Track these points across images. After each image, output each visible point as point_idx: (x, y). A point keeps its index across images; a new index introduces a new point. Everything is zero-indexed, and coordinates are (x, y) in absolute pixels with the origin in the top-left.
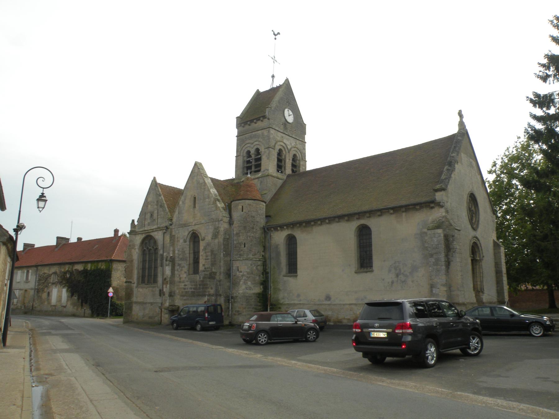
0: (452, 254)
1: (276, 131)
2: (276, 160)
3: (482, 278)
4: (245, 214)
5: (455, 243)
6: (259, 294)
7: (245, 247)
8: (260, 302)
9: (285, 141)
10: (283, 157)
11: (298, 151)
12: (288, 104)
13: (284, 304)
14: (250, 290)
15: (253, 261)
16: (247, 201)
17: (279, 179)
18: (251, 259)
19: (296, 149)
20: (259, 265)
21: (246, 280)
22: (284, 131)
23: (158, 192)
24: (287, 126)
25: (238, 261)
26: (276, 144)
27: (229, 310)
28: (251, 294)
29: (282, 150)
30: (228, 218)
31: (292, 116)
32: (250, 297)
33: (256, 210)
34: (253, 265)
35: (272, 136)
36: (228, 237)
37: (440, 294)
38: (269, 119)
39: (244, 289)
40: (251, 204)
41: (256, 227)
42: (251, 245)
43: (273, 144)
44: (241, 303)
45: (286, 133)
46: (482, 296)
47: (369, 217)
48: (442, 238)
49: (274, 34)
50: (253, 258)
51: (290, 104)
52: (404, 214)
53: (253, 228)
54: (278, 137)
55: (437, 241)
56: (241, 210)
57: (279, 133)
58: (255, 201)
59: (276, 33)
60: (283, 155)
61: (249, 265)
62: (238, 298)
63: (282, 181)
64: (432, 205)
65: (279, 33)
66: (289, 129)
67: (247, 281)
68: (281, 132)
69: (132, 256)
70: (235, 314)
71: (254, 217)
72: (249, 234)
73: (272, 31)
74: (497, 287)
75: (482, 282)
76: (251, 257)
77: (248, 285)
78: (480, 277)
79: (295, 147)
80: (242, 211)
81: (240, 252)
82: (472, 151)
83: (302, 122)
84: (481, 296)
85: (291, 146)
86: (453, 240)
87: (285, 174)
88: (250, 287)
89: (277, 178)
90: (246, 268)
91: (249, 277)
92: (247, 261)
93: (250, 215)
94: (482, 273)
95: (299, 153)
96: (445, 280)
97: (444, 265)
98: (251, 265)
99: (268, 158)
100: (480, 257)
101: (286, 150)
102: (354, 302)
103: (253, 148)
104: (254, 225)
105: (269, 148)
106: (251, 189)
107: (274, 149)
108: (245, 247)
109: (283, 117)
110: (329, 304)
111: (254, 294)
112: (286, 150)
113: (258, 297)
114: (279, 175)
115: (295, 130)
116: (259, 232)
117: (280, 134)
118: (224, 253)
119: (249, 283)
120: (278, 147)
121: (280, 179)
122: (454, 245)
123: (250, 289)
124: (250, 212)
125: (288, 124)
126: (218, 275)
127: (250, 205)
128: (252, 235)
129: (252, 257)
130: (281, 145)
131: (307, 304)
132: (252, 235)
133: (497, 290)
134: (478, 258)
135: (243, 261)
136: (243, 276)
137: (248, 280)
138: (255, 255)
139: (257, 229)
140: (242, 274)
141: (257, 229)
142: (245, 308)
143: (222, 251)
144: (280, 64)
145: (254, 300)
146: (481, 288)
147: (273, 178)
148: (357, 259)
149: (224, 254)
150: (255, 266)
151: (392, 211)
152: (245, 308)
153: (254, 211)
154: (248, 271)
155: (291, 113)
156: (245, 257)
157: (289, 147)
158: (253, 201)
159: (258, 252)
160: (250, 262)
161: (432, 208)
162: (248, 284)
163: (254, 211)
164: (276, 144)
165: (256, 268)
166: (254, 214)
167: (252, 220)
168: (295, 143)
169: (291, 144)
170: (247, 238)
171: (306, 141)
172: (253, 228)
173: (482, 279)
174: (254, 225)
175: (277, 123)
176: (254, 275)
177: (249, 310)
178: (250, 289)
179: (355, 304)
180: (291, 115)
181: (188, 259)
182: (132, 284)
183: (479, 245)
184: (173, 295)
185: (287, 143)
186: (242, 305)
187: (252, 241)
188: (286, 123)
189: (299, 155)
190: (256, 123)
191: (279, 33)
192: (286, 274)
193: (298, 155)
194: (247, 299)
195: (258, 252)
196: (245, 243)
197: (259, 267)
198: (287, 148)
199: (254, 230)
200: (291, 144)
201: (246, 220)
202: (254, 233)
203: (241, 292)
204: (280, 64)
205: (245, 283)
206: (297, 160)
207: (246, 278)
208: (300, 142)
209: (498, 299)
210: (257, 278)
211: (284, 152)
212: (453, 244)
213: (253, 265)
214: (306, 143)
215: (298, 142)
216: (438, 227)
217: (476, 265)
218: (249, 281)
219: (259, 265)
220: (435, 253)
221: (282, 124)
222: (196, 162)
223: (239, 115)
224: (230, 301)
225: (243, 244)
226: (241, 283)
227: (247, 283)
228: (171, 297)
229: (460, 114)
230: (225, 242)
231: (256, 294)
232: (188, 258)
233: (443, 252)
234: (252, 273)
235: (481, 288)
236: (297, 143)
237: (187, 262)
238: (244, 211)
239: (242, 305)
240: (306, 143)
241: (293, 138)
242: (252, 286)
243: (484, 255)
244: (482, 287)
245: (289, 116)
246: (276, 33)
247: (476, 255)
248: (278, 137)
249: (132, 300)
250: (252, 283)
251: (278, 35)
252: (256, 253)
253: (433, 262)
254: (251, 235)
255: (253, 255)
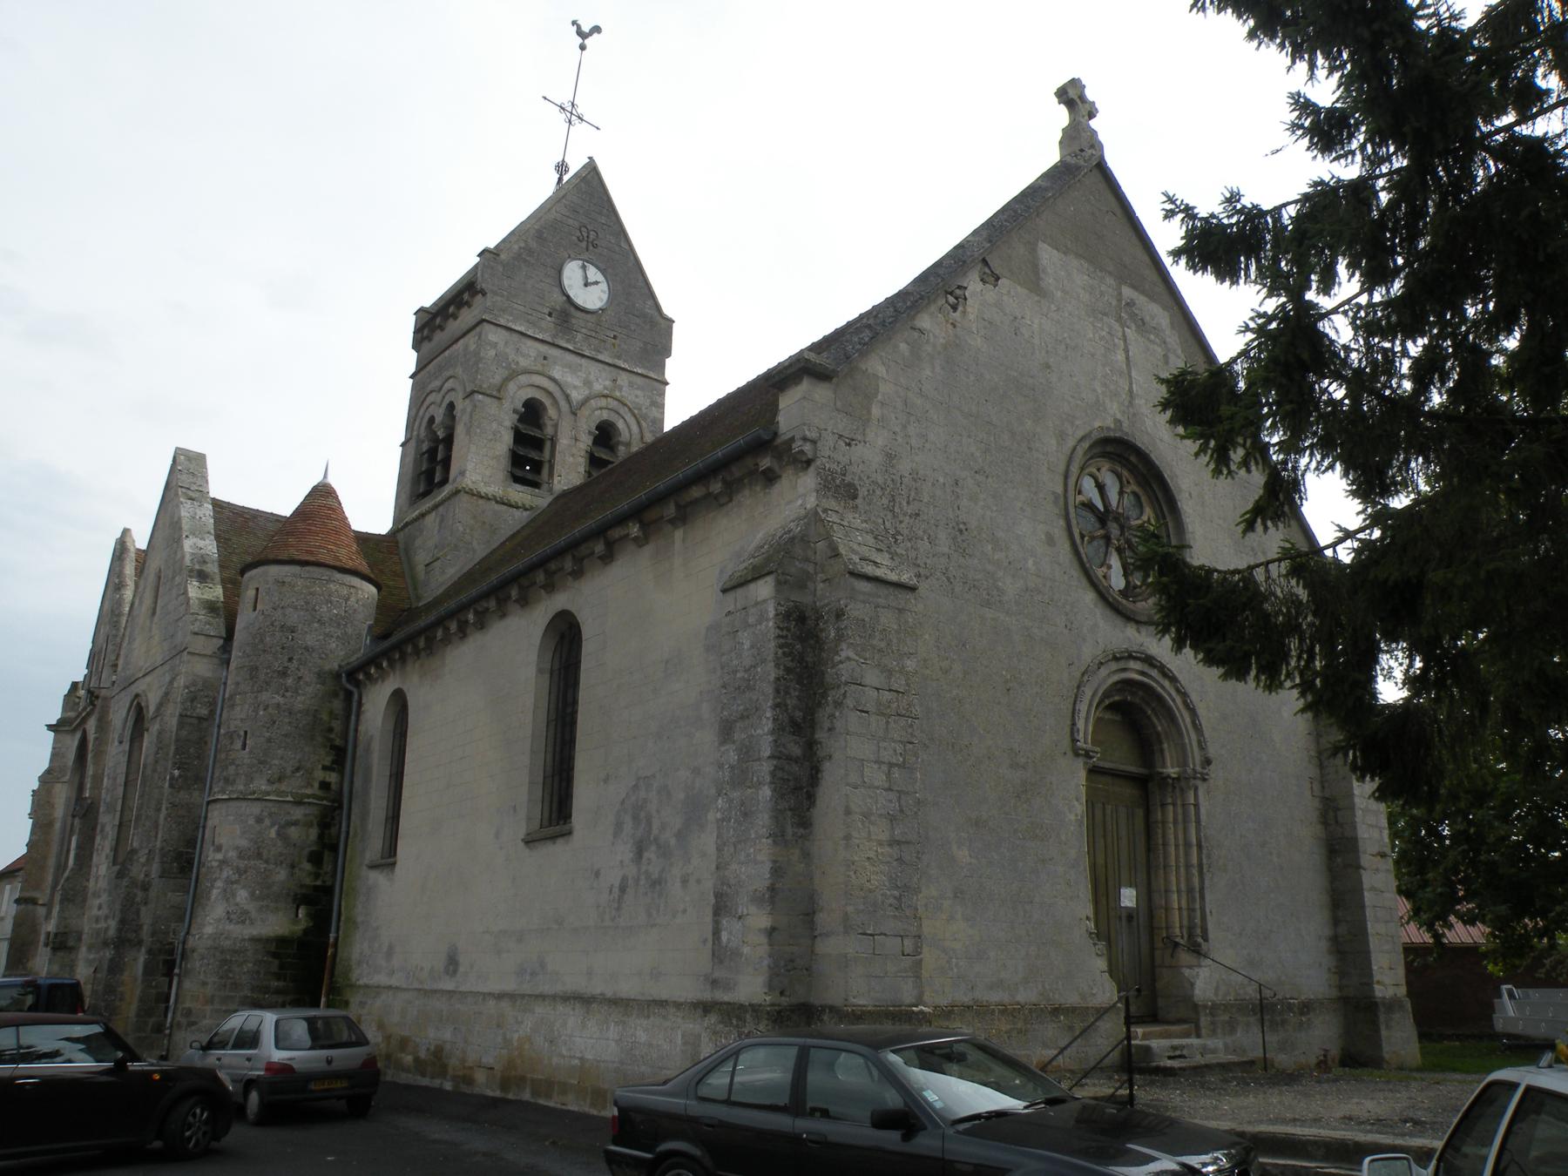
0: (832, 716)
1: (515, 337)
2: (507, 438)
3: (1195, 872)
4: (261, 618)
5: (843, 654)
6: (281, 941)
7: (244, 747)
8: (278, 977)
9: (557, 373)
10: (549, 430)
11: (621, 412)
12: (584, 244)
13: (367, 986)
14: (243, 922)
15: (270, 804)
16: (274, 570)
17: (511, 506)
18: (260, 796)
19: (613, 404)
20: (295, 823)
21: (232, 883)
22: (555, 336)
23: (118, 577)
24: (574, 321)
25: (218, 806)
26: (507, 379)
27: (167, 1008)
28: (244, 940)
29: (541, 403)
30: (215, 640)
31: (604, 286)
32: (235, 952)
33: (307, 603)
34: (267, 822)
35: (492, 353)
36: (204, 712)
37: (746, 950)
38: (484, 294)
39: (219, 920)
40: (286, 580)
41: (298, 669)
42: (269, 740)
43: (497, 379)
44: (202, 977)
45: (565, 345)
46: (1190, 967)
47: (578, 574)
48: (771, 624)
49: (580, 33)
50: (268, 793)
51: (595, 246)
52: (679, 534)
53: (284, 674)
54: (526, 356)
55: (752, 647)
56: (252, 605)
57: (530, 343)
58: (307, 568)
59: (586, 29)
60: (549, 423)
61: (251, 821)
62: (195, 954)
63: (526, 514)
64: (766, 462)
65: (597, 29)
66: (583, 330)
67: (235, 886)
68: (536, 339)
69: (53, 807)
70: (179, 1025)
71: (293, 632)
72: (264, 696)
73: (574, 23)
74: (1336, 922)
75: (1195, 895)
76: (263, 787)
77: (237, 904)
78: (1188, 866)
79: (606, 396)
80: (255, 610)
81: (227, 768)
82: (1146, 259)
83: (654, 312)
84: (1187, 972)
85: (587, 392)
86: (840, 637)
87: (550, 490)
88: (246, 912)
89: (497, 502)
90: (238, 832)
91: (245, 872)
92: (244, 804)
93: (276, 623)
94: (1200, 846)
95: (629, 417)
96: (768, 865)
97: (768, 778)
98: (259, 820)
99: (468, 432)
100: (1183, 763)
101: (563, 403)
102: (510, 986)
103: (440, 406)
104: (290, 659)
105: (473, 392)
106: (309, 525)
107: (499, 399)
108: (244, 747)
109: (557, 290)
110: (449, 991)
111: (253, 940)
112: (563, 403)
113: (275, 955)
114: (519, 494)
115: (615, 337)
116: (310, 690)
117: (532, 348)
118: (176, 772)
119: (242, 895)
120: (518, 394)
121: (517, 508)
122: (841, 662)
123: (244, 917)
124: (280, 611)
125: (579, 314)
126: (143, 860)
127: (284, 582)
128: (278, 699)
129: (269, 788)
130: (538, 387)
131: (405, 990)
132: (278, 699)
133: (1334, 939)
134: (1172, 771)
135: (231, 804)
136: (223, 862)
137: (236, 882)
138: (280, 780)
139: (300, 678)
140: (219, 856)
141: (300, 678)
142: (211, 1001)
143: (170, 764)
144: (545, 98)
145: (250, 965)
146: (1191, 929)
147: (481, 502)
148: (541, 779)
149: (172, 778)
150: (273, 825)
151: (634, 530)
152: (211, 1001)
153: (296, 608)
154: (244, 843)
155: (594, 274)
156: (241, 787)
157: (576, 396)
158: (296, 569)
159: (298, 769)
160: (256, 809)
161: (770, 478)
162: (238, 899)
163: (296, 608)
164: (507, 379)
165: (278, 834)
166: (293, 618)
167: (284, 640)
168: (608, 383)
169: (588, 383)
170: (256, 711)
171: (668, 375)
172: (284, 674)
173: (1196, 881)
174: (290, 659)
175: (521, 308)
176: (267, 862)
177: (224, 1008)
178: (244, 917)
179: (512, 997)
180: (596, 283)
181: (119, 808)
182: (38, 907)
183: (1176, 703)
184: (71, 943)
185: (568, 378)
186: (204, 984)
187: (274, 722)
188: (572, 309)
189: (628, 427)
190: (455, 317)
191: (597, 29)
192: (382, 858)
193: (621, 425)
194: (224, 962)
195: (298, 769)
196: (246, 733)
197: (294, 832)
198: (567, 397)
199: (290, 681)
200: (588, 383)
201: (262, 641)
202: (288, 694)
203: (209, 930)
204: (545, 98)
205: (228, 895)
206: (619, 443)
207: (231, 872)
208: (639, 380)
209: (1340, 988)
210: (281, 875)
211: (552, 412)
212: (837, 658)
213: (267, 822)
214: (667, 384)
215: (623, 379)
216: (756, 575)
217: (1163, 805)
218: (244, 887)
219: (295, 823)
220: (742, 717)
221: (546, 311)
222: (177, 449)
223: (427, 304)
224: (176, 971)
225: (239, 736)
226: (215, 892)
227: (234, 895)
228: (60, 954)
229: (1072, 96)
230: (184, 733)
231: (268, 940)
232: (120, 802)
233: (770, 703)
234: (259, 855)
235: (1191, 929)
236: (619, 382)
237: (114, 818)
238: (259, 607)
239: (204, 984)
240: (667, 384)
241: (601, 365)
242: (251, 907)
243: (1212, 751)
244: (1198, 921)
245: (586, 284)
246: (586, 29)
247: (1162, 751)
248: (526, 356)
249: (30, 965)
250: (252, 894)
251: (595, 35)
252: (288, 772)
253: (732, 767)
254: (274, 701)
255: (270, 782)
